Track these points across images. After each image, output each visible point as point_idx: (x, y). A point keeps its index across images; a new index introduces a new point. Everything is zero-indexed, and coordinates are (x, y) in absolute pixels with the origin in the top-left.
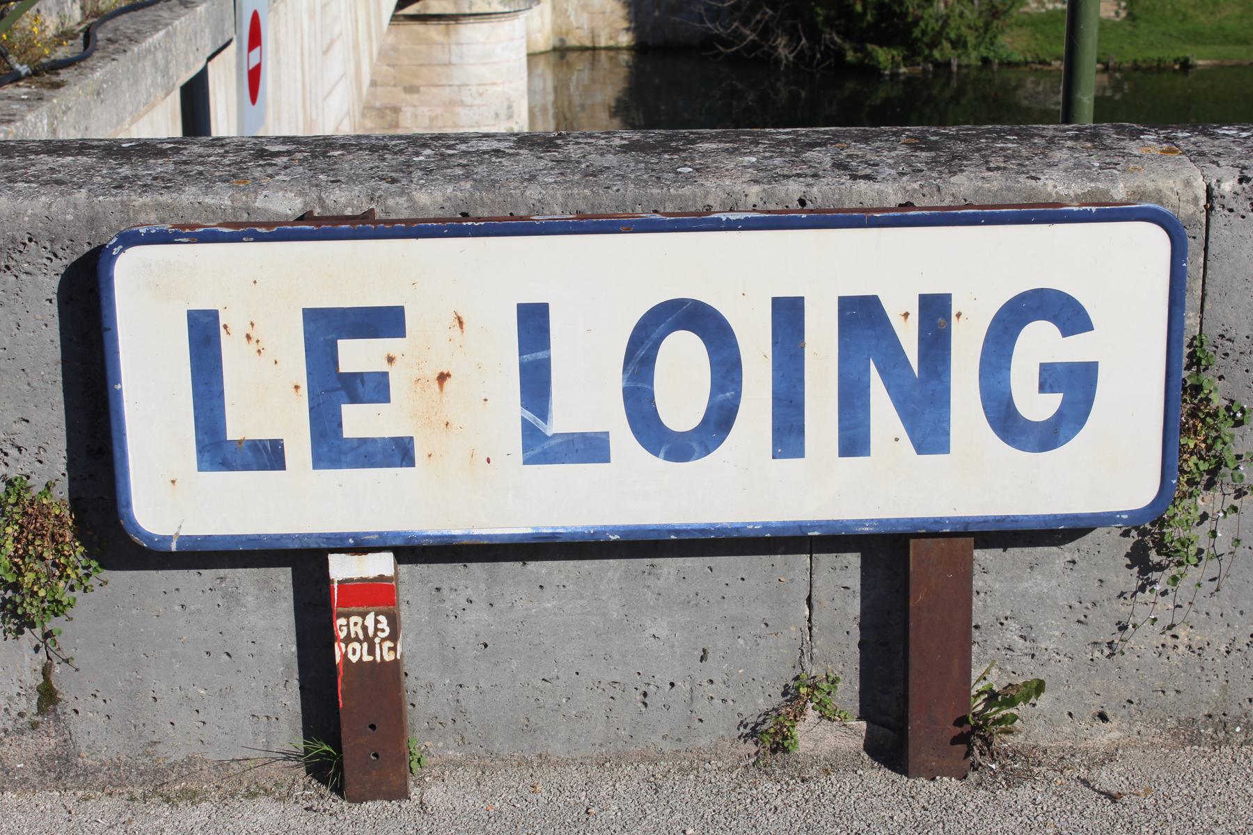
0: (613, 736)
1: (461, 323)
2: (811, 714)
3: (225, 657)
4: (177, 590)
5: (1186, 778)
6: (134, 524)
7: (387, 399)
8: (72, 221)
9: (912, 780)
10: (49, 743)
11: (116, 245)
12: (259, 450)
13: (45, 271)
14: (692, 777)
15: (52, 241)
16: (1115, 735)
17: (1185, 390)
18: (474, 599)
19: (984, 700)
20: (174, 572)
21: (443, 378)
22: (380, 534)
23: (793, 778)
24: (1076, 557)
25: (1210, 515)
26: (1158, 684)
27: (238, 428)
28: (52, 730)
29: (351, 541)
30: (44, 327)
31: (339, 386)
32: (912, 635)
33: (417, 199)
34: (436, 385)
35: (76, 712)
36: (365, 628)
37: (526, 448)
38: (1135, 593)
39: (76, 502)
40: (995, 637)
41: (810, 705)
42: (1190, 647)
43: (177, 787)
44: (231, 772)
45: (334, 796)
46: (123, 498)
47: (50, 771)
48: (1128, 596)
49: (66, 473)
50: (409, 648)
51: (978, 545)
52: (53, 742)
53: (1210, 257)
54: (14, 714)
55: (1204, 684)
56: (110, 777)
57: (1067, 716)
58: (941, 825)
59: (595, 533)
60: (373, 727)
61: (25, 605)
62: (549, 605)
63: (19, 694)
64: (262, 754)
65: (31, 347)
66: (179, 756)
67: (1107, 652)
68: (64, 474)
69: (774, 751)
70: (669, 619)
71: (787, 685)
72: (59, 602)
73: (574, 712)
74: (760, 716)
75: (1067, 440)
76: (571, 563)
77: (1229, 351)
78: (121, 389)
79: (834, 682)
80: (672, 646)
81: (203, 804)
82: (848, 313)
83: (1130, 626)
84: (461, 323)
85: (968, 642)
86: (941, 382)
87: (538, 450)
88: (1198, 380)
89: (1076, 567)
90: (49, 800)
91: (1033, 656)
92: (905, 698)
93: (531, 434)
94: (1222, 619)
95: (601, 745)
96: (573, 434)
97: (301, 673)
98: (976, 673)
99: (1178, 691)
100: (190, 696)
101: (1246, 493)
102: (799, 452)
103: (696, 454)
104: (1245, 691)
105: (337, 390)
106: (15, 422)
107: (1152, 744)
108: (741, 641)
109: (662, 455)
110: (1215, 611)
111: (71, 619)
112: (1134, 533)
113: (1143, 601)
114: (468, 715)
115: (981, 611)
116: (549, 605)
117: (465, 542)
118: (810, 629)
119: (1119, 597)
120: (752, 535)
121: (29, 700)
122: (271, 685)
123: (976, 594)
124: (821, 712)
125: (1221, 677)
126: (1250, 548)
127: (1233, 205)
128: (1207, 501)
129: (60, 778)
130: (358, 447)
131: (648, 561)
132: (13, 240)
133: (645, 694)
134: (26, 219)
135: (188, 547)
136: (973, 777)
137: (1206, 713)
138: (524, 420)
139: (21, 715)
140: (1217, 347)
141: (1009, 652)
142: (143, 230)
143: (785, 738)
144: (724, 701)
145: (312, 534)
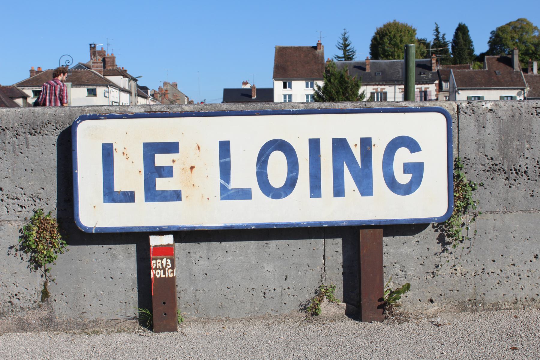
0: (253, 310)
1: (199, 148)
2: (326, 300)
3: (111, 279)
4: (94, 253)
5: (463, 320)
6: (80, 223)
7: (172, 176)
8: (64, 116)
9: (363, 323)
10: (45, 313)
11: (78, 120)
12: (126, 195)
13: (53, 134)
14: (282, 324)
15: (56, 123)
16: (436, 308)
17: (454, 178)
18: (202, 256)
19: (389, 295)
20: (93, 246)
21: (192, 168)
22: (169, 226)
23: (319, 323)
24: (419, 240)
25: (466, 224)
26: (451, 288)
27: (118, 187)
28: (46, 308)
29: (158, 229)
30: (51, 154)
31: (155, 171)
32: (362, 266)
33: (184, 108)
34: (189, 171)
35: (55, 301)
36: (162, 264)
37: (222, 194)
38: (441, 253)
39: (59, 219)
40: (392, 270)
41: (325, 297)
42: (461, 274)
43: (91, 330)
44: (112, 324)
45: (149, 331)
46: (76, 213)
47: (44, 324)
48: (438, 254)
49: (56, 208)
50: (178, 275)
51: (386, 235)
52: (46, 312)
53: (460, 129)
54: (32, 301)
55: (467, 288)
56: (67, 326)
57: (419, 301)
58: (375, 334)
59: (246, 226)
60: (164, 303)
61: (38, 257)
62: (230, 259)
63: (35, 294)
64: (123, 317)
65: (46, 162)
66: (92, 318)
67: (432, 276)
68: (55, 209)
69: (312, 315)
70: (273, 264)
71: (316, 289)
72: (50, 257)
73: (239, 301)
74: (307, 302)
75: (414, 191)
76: (237, 243)
77: (468, 163)
78: (77, 172)
79: (333, 288)
80: (274, 275)
81: (101, 335)
82: (336, 144)
83: (440, 266)
84: (199, 148)
85: (382, 273)
86: (369, 169)
87: (226, 195)
88: (458, 173)
89: (419, 243)
90: (44, 335)
91: (405, 277)
92: (360, 294)
93: (223, 189)
94: (472, 263)
95: (249, 313)
96: (238, 189)
97: (138, 285)
98: (385, 284)
99: (458, 291)
100: (97, 294)
101: (477, 215)
102: (319, 196)
103: (283, 196)
104: (482, 290)
105: (155, 172)
106: (39, 189)
107: (450, 311)
108: (299, 273)
109: (270, 197)
110: (469, 260)
111: (55, 264)
112: (439, 230)
113: (443, 256)
114: (199, 301)
115: (387, 260)
116: (230, 259)
117: (199, 229)
118: (324, 268)
119: (435, 255)
120: (303, 226)
121: (38, 296)
122: (127, 290)
123: (384, 254)
124: (329, 299)
125: (473, 285)
126: (480, 236)
127: (466, 111)
128: (465, 218)
129: (48, 327)
130: (162, 194)
131: (265, 242)
132: (42, 123)
133: (265, 293)
134: (48, 115)
135: (98, 231)
136: (386, 321)
137: (468, 299)
138: (221, 184)
139: (35, 302)
140: (464, 162)
141: (397, 276)
142: (88, 115)
143: (316, 309)
144: (294, 296)
145: (144, 227)
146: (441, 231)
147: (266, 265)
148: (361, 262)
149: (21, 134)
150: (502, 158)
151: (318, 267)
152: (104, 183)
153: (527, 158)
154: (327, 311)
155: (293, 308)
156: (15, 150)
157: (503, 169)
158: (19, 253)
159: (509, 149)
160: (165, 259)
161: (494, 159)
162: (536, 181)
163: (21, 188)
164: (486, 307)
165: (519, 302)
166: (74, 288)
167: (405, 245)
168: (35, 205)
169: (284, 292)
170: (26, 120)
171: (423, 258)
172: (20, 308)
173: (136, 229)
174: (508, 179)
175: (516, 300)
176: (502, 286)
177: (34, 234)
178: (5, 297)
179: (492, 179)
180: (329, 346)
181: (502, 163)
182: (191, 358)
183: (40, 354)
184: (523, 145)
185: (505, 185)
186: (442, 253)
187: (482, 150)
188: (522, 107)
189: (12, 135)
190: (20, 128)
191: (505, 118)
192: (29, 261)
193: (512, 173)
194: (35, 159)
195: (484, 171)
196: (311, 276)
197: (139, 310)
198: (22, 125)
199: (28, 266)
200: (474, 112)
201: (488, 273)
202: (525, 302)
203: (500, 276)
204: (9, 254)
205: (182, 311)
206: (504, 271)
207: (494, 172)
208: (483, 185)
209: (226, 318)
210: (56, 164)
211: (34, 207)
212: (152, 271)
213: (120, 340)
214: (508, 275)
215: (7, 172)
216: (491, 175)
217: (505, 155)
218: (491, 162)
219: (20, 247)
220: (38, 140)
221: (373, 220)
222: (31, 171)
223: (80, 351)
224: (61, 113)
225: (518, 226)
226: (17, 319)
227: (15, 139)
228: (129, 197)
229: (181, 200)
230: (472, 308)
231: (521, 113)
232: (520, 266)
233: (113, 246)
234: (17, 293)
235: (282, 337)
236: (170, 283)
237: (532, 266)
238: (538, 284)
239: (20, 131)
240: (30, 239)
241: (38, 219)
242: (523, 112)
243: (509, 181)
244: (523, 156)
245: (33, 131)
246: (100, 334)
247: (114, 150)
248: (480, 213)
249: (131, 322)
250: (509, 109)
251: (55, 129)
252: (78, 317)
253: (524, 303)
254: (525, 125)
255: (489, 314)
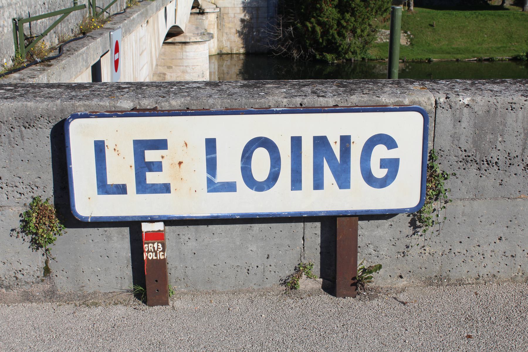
0: (238, 284)
1: (186, 145)
2: (304, 276)
3: (107, 257)
6: (76, 212)
7: (161, 170)
8: (56, 110)
9: (337, 298)
10: (47, 286)
11: (70, 118)
14: (264, 297)
15: (49, 117)
16: (405, 283)
17: (428, 167)
18: (190, 238)
20: (90, 229)
21: (180, 163)
23: (298, 298)
24: (392, 224)
26: (419, 266)
28: (48, 282)
29: (149, 218)
31: (145, 166)
33: (172, 103)
34: (178, 165)
35: (57, 276)
36: (154, 248)
38: (412, 235)
39: (56, 205)
41: (303, 273)
43: (91, 301)
46: (72, 204)
47: (48, 296)
50: (169, 254)
51: (360, 220)
52: (49, 286)
53: (436, 123)
54: (36, 277)
55: (434, 265)
56: (68, 298)
57: (389, 277)
58: (347, 313)
59: (231, 215)
60: (157, 281)
61: (39, 240)
63: (37, 270)
64: (119, 290)
66: (91, 291)
67: (402, 255)
68: (52, 196)
69: (291, 289)
70: (256, 245)
71: (296, 267)
72: (51, 239)
77: (442, 155)
78: (72, 167)
80: (257, 254)
81: (100, 307)
82: (316, 142)
83: (410, 246)
84: (186, 145)
85: (356, 252)
86: (347, 165)
87: (212, 188)
88: (432, 164)
89: (392, 227)
90: (48, 306)
92: (335, 271)
93: (210, 182)
95: (233, 287)
97: (132, 263)
98: (359, 262)
100: (95, 270)
101: (448, 202)
102: (300, 188)
103: (266, 189)
107: (417, 286)
108: (280, 252)
109: (254, 189)
110: (438, 241)
111: (55, 245)
112: (411, 215)
115: (361, 242)
117: (188, 219)
118: (304, 248)
119: (406, 237)
120: (284, 216)
121: (41, 272)
122: (122, 267)
124: (307, 276)
127: (444, 106)
128: (436, 205)
129: (51, 298)
131: (249, 225)
133: (248, 270)
135: (94, 220)
136: (358, 297)
139: (38, 277)
140: (439, 153)
141: (370, 255)
142: (79, 113)
143: (295, 284)
146: (413, 216)
147: (250, 246)
148: (337, 246)
149: (16, 127)
150: (475, 150)
151: (298, 248)
152: (97, 177)
153: (499, 150)
154: (305, 285)
155: (274, 283)
156: (11, 142)
157: (475, 160)
158: (20, 235)
159: (482, 142)
160: (156, 243)
161: (467, 151)
162: (506, 171)
163: (19, 177)
164: (450, 282)
165: (481, 278)
166: (73, 265)
167: (379, 229)
168: (33, 192)
169: (266, 269)
170: (19, 114)
171: (395, 239)
172: (24, 282)
173: (128, 218)
174: (479, 169)
175: (479, 276)
176: (467, 264)
177: (34, 220)
178: (10, 273)
179: (464, 169)
180: (305, 329)
181: (475, 155)
182: (182, 340)
183: (46, 332)
184: (496, 138)
185: (476, 175)
186: (413, 236)
187: (456, 142)
188: (498, 103)
189: (7, 128)
190: (14, 122)
191: (480, 113)
192: (30, 242)
193: (483, 164)
194: (30, 151)
195: (457, 162)
196: (291, 255)
197: (134, 287)
198: (16, 119)
199: (30, 246)
200: (451, 107)
201: (454, 253)
202: (487, 278)
203: (466, 255)
204: (11, 236)
205: (173, 285)
206: (469, 251)
207: (467, 163)
208: (456, 174)
209: (213, 291)
210: (50, 156)
211: (32, 193)
212: (144, 253)
213: (118, 315)
214: (473, 255)
215: (5, 163)
216: (463, 165)
217: (477, 147)
218: (464, 154)
219: (21, 230)
220: (32, 133)
221: (350, 211)
222: (27, 161)
223: (82, 327)
224: (53, 108)
225: (485, 211)
226: (23, 291)
227: (10, 132)
228: (122, 189)
229: (170, 192)
230: (438, 283)
231: (496, 108)
232: (485, 247)
233: (107, 228)
234: (21, 270)
235: (263, 316)
236: (161, 265)
237: (495, 246)
238: (500, 262)
239: (15, 124)
240: (30, 225)
241: (36, 206)
242: (499, 107)
243: (480, 171)
244: (496, 148)
245: (27, 125)
246: (99, 306)
247: (106, 147)
248: (451, 201)
249: (127, 295)
250: (485, 105)
251: (48, 122)
252: (78, 290)
253: (486, 279)
254: (499, 119)
255: (453, 290)
